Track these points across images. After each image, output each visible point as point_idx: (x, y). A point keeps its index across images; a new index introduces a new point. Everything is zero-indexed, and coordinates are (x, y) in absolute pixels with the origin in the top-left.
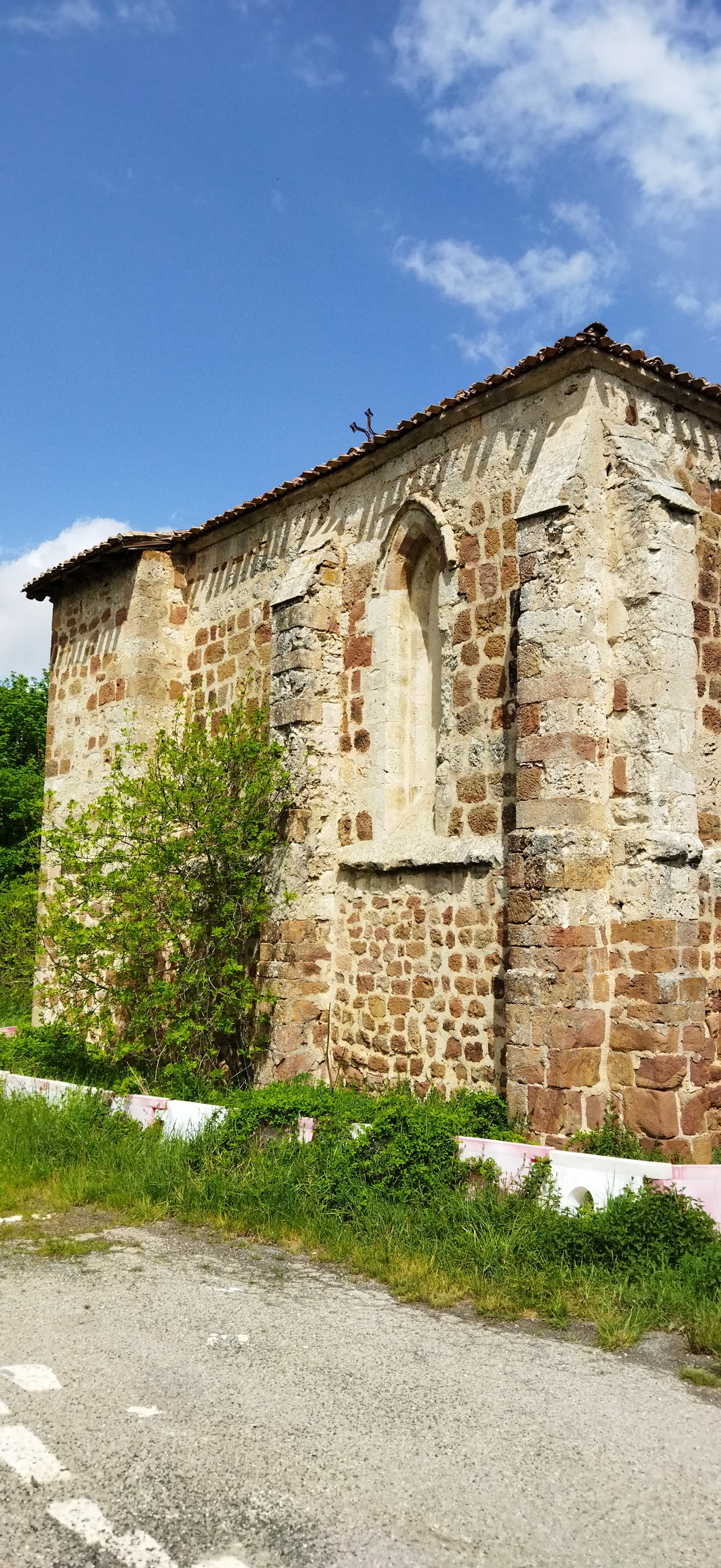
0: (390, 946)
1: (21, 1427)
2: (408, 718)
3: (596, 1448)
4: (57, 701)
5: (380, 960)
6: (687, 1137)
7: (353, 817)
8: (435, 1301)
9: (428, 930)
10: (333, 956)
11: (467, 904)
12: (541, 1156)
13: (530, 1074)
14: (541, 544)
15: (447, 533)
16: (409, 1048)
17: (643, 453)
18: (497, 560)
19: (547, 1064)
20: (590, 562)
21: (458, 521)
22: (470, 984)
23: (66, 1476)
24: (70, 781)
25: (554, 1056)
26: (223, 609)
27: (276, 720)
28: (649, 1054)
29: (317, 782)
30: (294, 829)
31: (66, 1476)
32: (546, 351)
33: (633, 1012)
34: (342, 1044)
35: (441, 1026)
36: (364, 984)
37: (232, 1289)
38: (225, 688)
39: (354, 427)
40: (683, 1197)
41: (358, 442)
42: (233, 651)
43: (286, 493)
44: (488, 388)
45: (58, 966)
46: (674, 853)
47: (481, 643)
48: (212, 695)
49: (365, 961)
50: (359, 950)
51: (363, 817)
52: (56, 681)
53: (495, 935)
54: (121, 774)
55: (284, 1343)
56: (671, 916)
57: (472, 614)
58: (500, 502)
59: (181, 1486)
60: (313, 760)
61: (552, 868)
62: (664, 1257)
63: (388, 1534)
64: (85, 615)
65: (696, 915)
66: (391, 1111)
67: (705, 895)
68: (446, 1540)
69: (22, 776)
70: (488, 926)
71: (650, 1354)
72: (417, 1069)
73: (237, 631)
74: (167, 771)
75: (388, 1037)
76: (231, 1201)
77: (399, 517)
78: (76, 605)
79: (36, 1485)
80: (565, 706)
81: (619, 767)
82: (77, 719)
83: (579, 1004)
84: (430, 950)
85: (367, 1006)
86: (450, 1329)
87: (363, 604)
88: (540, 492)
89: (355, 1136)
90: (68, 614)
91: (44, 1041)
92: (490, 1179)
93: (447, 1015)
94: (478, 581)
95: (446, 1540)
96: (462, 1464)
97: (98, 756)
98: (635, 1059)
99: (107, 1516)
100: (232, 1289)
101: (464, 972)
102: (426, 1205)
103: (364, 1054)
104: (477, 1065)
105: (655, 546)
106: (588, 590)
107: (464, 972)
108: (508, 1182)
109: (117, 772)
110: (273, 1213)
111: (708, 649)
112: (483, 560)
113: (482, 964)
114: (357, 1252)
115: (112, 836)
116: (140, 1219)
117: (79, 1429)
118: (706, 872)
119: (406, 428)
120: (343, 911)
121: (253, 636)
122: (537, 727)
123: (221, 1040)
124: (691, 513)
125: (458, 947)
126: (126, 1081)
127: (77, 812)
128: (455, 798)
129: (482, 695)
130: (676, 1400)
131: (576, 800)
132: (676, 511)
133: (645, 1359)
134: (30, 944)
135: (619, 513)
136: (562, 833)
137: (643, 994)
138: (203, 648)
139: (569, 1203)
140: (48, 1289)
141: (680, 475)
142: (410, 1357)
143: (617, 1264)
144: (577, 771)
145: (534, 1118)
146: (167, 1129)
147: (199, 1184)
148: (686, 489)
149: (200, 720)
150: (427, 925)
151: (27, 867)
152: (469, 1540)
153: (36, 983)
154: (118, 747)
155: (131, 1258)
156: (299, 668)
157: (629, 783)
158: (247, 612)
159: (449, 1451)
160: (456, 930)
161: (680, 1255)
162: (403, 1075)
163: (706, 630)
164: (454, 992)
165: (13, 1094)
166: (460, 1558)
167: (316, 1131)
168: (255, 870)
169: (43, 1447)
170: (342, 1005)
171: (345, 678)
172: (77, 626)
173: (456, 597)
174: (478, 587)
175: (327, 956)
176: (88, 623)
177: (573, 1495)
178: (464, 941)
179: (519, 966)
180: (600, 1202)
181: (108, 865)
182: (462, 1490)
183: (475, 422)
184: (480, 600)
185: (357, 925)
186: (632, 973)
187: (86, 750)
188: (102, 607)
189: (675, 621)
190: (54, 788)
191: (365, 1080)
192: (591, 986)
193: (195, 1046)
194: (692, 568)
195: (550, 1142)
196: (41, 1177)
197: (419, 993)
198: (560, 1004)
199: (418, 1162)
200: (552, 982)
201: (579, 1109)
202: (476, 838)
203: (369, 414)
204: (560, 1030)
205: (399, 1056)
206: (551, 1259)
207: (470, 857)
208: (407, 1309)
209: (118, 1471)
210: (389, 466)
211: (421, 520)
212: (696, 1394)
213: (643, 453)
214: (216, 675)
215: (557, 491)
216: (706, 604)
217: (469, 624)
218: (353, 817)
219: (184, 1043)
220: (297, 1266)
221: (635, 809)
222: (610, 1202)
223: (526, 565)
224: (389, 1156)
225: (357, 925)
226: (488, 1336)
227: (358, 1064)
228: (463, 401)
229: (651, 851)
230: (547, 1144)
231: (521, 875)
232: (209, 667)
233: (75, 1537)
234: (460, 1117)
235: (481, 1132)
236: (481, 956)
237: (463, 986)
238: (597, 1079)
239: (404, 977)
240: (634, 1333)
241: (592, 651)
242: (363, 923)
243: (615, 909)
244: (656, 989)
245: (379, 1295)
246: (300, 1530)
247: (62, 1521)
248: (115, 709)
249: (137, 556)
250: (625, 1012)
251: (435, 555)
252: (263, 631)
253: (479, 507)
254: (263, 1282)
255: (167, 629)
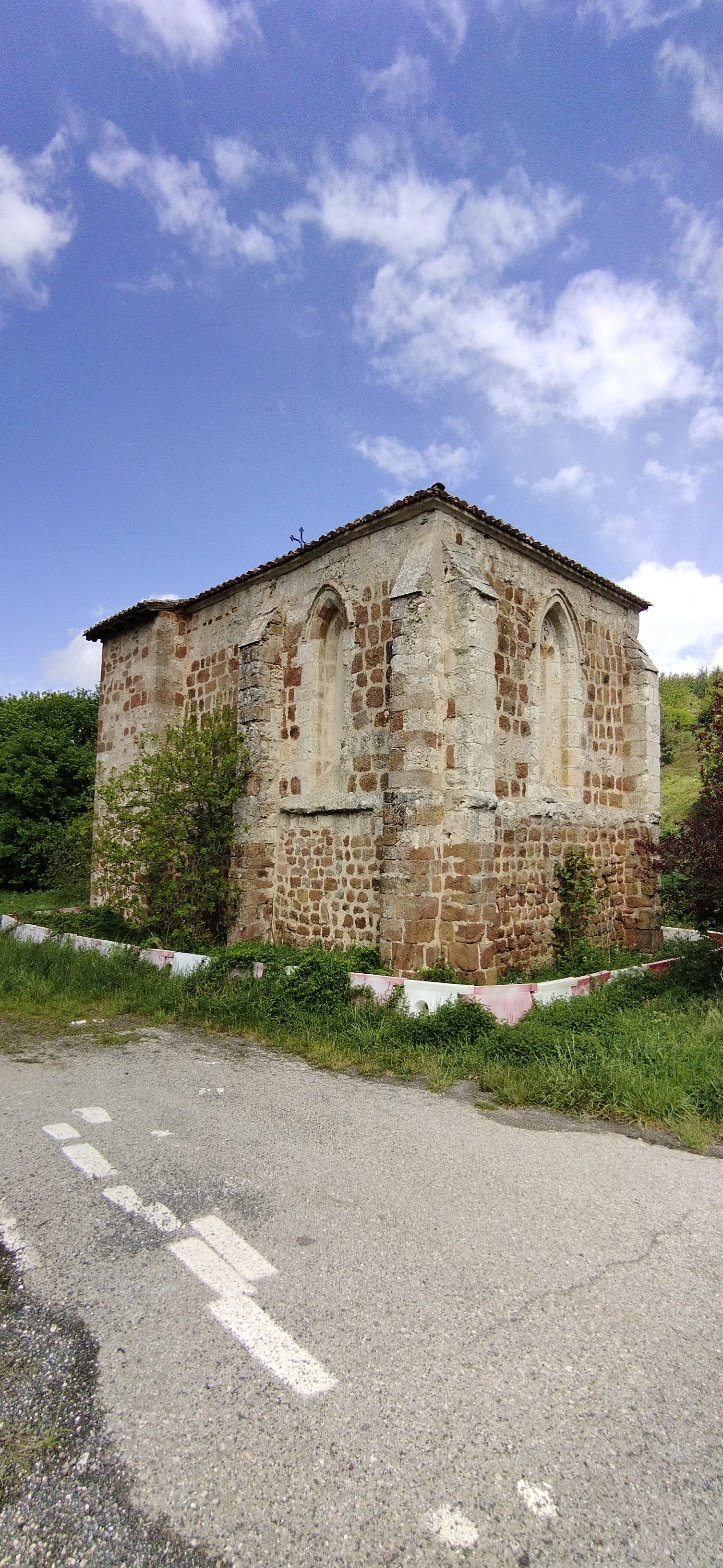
0: (310, 860)
1: (87, 1144)
2: (324, 719)
3: (425, 1147)
4: (104, 705)
5: (305, 868)
6: (484, 970)
7: (289, 780)
8: (334, 1067)
9: (334, 850)
10: (276, 866)
11: (358, 834)
12: (399, 984)
13: (394, 935)
14: (405, 614)
15: (348, 605)
16: (321, 921)
17: (466, 562)
18: (379, 623)
19: (404, 930)
20: (434, 626)
21: (355, 598)
22: (359, 881)
23: (114, 1172)
24: (113, 755)
25: (408, 925)
26: (209, 648)
27: (241, 718)
28: (464, 923)
29: (266, 758)
30: (251, 786)
31: (114, 1172)
32: (409, 498)
33: (455, 898)
34: (281, 918)
35: (341, 907)
36: (295, 883)
37: (214, 1063)
38: (210, 698)
39: (292, 538)
40: (480, 1004)
41: (295, 547)
42: (215, 674)
43: (249, 577)
44: (374, 518)
45: (106, 870)
46: (481, 803)
47: (368, 673)
48: (201, 702)
49: (296, 868)
50: (292, 862)
51: (295, 780)
52: (104, 692)
53: (375, 852)
54: (144, 752)
55: (245, 1093)
56: (479, 841)
57: (364, 656)
58: (381, 588)
59: (183, 1176)
60: (264, 745)
61: (409, 812)
62: (467, 1039)
63: (305, 1200)
64: (123, 651)
65: (493, 841)
66: (310, 958)
67: (499, 829)
68: (338, 1202)
69: (84, 752)
70: (371, 847)
71: (458, 1093)
72: (326, 933)
73: (217, 663)
74: (173, 750)
75: (309, 915)
76: (213, 1011)
77: (319, 594)
78: (117, 645)
79: (95, 1178)
80: (418, 713)
81: (450, 751)
82: (117, 717)
83: (424, 894)
84: (335, 863)
85: (296, 896)
86: (343, 1083)
87: (296, 647)
88: (405, 582)
89: (288, 973)
90: (112, 650)
91: (97, 915)
92: (369, 997)
93: (345, 900)
94: (367, 635)
95: (338, 1202)
96: (348, 1158)
97: (129, 739)
98: (455, 926)
99: (139, 1195)
100: (214, 1063)
101: (355, 875)
102: (331, 1013)
103: (295, 924)
104: (362, 931)
105: (472, 618)
106: (433, 643)
107: (355, 875)
108: (379, 998)
109: (142, 750)
110: (238, 1019)
111: (502, 681)
112: (370, 623)
113: (366, 871)
114: (289, 1041)
115: (140, 790)
116: (158, 1023)
117: (122, 1145)
118: (499, 815)
119: (324, 540)
120: (282, 838)
121: (227, 666)
122: (402, 726)
123: (206, 915)
124: (494, 599)
125: (352, 860)
126: (148, 940)
127: (117, 774)
128: (352, 769)
129: (369, 705)
130: (472, 1118)
131: (424, 771)
132: (484, 596)
133: (454, 1095)
134: (89, 856)
135: (451, 597)
136: (416, 791)
137: (460, 888)
138: (197, 673)
139: (414, 1010)
140: (103, 1063)
141: (487, 576)
142: (320, 1099)
143: (441, 1043)
144: (426, 753)
145: (395, 961)
146: (174, 970)
147: (194, 1002)
148: (491, 585)
149: (194, 718)
150: (333, 847)
151: (84, 809)
152: (352, 1201)
153: (92, 880)
154: (142, 735)
155: (153, 1045)
156: (256, 686)
157: (456, 761)
158: (224, 650)
159: (341, 1151)
160: (350, 849)
161: (477, 1037)
162: (318, 937)
163: (502, 670)
164: (349, 887)
165: (79, 948)
166: (347, 1211)
167: (265, 971)
168: (227, 811)
169: (100, 1156)
170: (281, 895)
171: (284, 693)
172: (118, 658)
173: (353, 644)
174: (367, 639)
175: (272, 865)
176: (124, 657)
177: (412, 1174)
178: (356, 856)
179: (388, 871)
180: (432, 1009)
181: (137, 808)
182: (349, 1173)
183: (366, 538)
184: (369, 647)
185: (291, 846)
186: (455, 875)
187: (122, 736)
188: (133, 646)
189: (484, 663)
190: (103, 760)
191: (295, 940)
192: (431, 883)
193: (192, 920)
194: (494, 632)
195: (405, 975)
196: (98, 998)
197: (328, 888)
198: (412, 894)
199: (326, 988)
200: (408, 881)
201: (422, 955)
202: (364, 793)
203: (301, 530)
204: (412, 909)
205: (316, 925)
206: (403, 1042)
207: (359, 805)
208: (318, 1072)
209: (146, 1168)
210: (313, 563)
211: (333, 597)
212: (483, 1115)
213: (466, 562)
214: (204, 690)
215: (415, 582)
216: (502, 654)
217: (361, 661)
218: (289, 780)
219: (184, 917)
220: (253, 1049)
221: (458, 777)
222: (438, 1008)
223: (396, 627)
224: (309, 985)
225: (291, 846)
226: (365, 1086)
227: (291, 930)
228: (359, 525)
229: (467, 802)
230: (403, 976)
231: (391, 817)
232: (200, 685)
233: (120, 1208)
234: (351, 962)
235: (364, 970)
236: (366, 865)
237: (354, 884)
238: (433, 938)
239: (319, 878)
240: (449, 1082)
241: (435, 680)
242: (294, 846)
243: (446, 837)
244: (469, 884)
245: (301, 1065)
246: (254, 1199)
247: (111, 1198)
248: (139, 710)
249: (156, 614)
250: (450, 898)
251: (342, 618)
252: (234, 664)
253: (368, 590)
254: (233, 1058)
255: (174, 661)
